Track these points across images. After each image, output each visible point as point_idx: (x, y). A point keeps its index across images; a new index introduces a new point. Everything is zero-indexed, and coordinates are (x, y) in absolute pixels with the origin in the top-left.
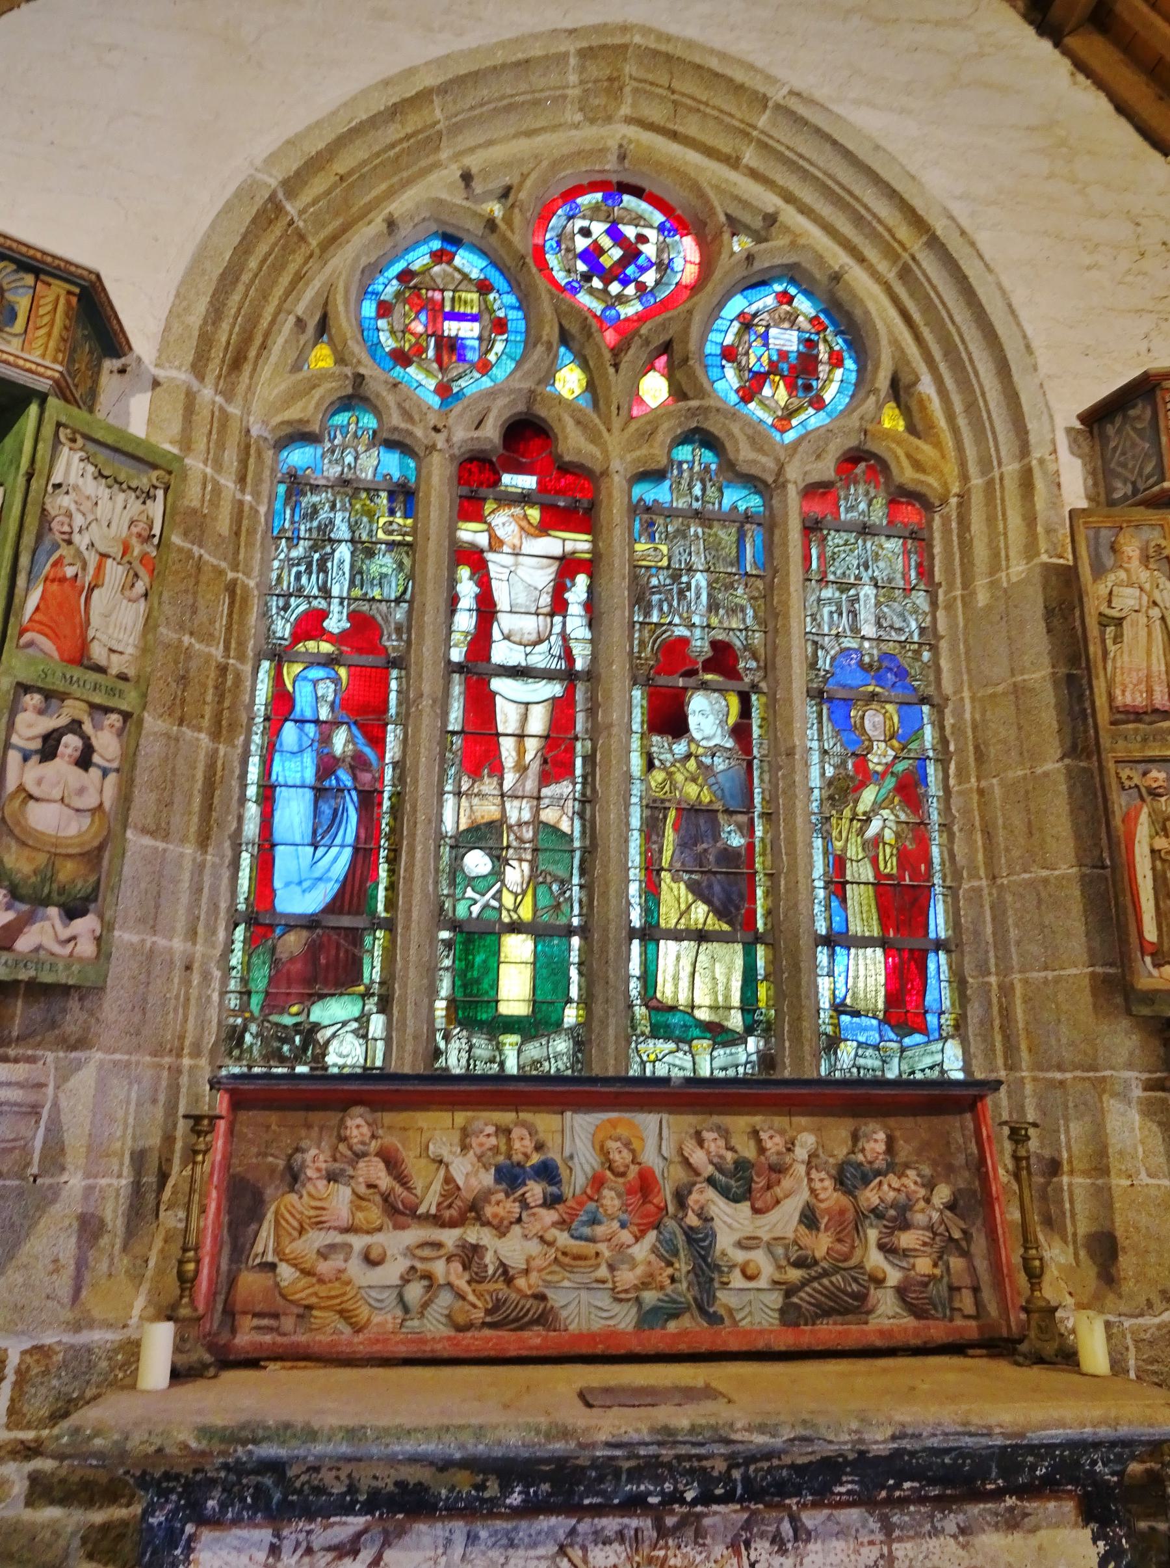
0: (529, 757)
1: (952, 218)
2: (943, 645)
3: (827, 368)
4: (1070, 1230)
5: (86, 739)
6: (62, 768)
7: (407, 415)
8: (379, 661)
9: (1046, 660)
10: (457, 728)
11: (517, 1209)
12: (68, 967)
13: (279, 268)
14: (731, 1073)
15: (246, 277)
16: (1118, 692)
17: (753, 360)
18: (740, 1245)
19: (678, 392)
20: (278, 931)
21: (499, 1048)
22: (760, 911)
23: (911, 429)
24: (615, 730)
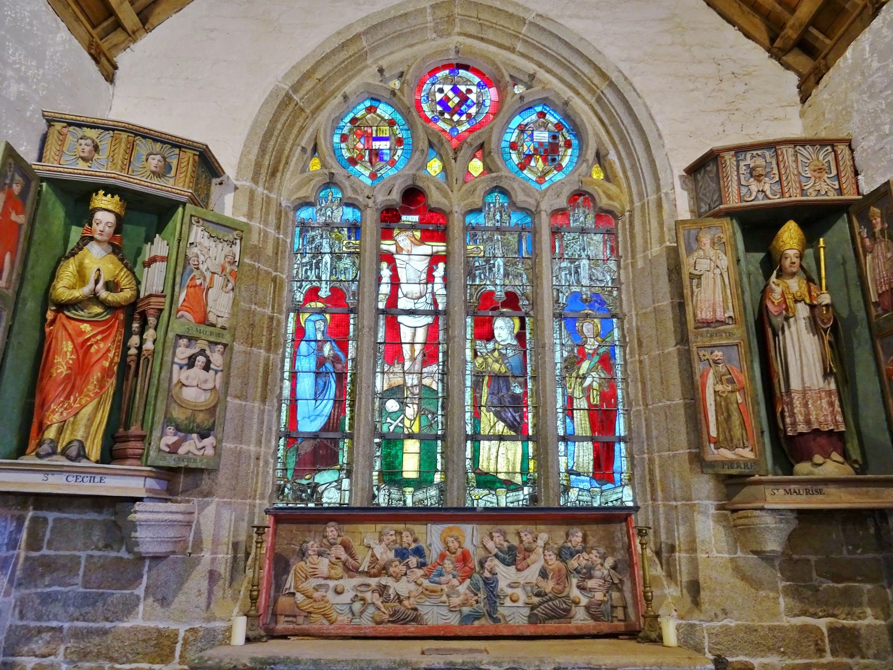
0: (417, 353)
1: (620, 72)
2: (623, 287)
3: (563, 149)
4: (679, 578)
5: (207, 357)
6: (197, 372)
7: (355, 191)
8: (345, 310)
9: (668, 295)
10: (382, 341)
11: (404, 569)
12: (201, 461)
13: (292, 125)
14: (516, 504)
15: (276, 133)
16: (699, 312)
17: (525, 148)
18: (510, 586)
19: (488, 169)
20: (299, 440)
21: (403, 494)
22: (530, 425)
23: (607, 178)
24: (456, 339)
